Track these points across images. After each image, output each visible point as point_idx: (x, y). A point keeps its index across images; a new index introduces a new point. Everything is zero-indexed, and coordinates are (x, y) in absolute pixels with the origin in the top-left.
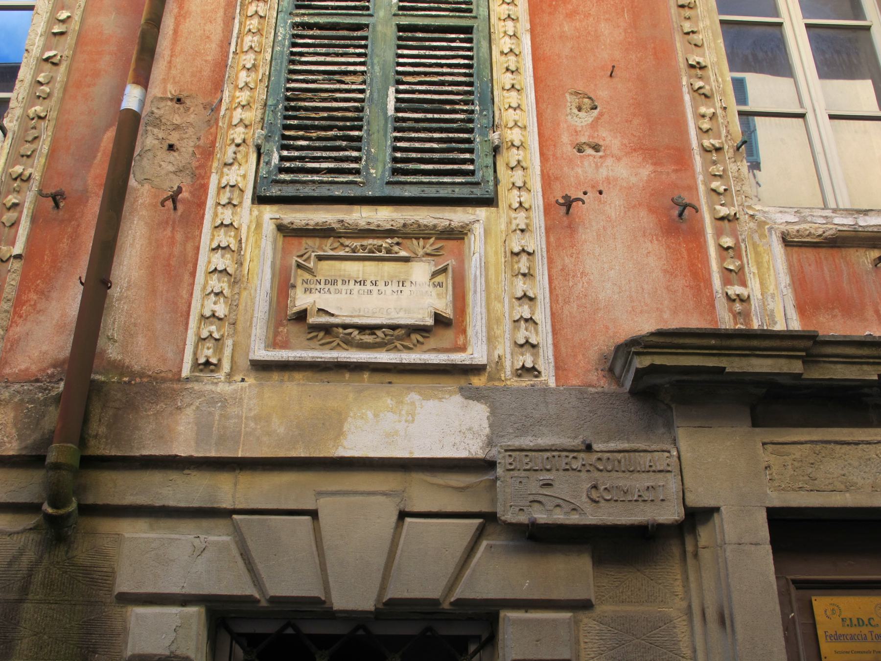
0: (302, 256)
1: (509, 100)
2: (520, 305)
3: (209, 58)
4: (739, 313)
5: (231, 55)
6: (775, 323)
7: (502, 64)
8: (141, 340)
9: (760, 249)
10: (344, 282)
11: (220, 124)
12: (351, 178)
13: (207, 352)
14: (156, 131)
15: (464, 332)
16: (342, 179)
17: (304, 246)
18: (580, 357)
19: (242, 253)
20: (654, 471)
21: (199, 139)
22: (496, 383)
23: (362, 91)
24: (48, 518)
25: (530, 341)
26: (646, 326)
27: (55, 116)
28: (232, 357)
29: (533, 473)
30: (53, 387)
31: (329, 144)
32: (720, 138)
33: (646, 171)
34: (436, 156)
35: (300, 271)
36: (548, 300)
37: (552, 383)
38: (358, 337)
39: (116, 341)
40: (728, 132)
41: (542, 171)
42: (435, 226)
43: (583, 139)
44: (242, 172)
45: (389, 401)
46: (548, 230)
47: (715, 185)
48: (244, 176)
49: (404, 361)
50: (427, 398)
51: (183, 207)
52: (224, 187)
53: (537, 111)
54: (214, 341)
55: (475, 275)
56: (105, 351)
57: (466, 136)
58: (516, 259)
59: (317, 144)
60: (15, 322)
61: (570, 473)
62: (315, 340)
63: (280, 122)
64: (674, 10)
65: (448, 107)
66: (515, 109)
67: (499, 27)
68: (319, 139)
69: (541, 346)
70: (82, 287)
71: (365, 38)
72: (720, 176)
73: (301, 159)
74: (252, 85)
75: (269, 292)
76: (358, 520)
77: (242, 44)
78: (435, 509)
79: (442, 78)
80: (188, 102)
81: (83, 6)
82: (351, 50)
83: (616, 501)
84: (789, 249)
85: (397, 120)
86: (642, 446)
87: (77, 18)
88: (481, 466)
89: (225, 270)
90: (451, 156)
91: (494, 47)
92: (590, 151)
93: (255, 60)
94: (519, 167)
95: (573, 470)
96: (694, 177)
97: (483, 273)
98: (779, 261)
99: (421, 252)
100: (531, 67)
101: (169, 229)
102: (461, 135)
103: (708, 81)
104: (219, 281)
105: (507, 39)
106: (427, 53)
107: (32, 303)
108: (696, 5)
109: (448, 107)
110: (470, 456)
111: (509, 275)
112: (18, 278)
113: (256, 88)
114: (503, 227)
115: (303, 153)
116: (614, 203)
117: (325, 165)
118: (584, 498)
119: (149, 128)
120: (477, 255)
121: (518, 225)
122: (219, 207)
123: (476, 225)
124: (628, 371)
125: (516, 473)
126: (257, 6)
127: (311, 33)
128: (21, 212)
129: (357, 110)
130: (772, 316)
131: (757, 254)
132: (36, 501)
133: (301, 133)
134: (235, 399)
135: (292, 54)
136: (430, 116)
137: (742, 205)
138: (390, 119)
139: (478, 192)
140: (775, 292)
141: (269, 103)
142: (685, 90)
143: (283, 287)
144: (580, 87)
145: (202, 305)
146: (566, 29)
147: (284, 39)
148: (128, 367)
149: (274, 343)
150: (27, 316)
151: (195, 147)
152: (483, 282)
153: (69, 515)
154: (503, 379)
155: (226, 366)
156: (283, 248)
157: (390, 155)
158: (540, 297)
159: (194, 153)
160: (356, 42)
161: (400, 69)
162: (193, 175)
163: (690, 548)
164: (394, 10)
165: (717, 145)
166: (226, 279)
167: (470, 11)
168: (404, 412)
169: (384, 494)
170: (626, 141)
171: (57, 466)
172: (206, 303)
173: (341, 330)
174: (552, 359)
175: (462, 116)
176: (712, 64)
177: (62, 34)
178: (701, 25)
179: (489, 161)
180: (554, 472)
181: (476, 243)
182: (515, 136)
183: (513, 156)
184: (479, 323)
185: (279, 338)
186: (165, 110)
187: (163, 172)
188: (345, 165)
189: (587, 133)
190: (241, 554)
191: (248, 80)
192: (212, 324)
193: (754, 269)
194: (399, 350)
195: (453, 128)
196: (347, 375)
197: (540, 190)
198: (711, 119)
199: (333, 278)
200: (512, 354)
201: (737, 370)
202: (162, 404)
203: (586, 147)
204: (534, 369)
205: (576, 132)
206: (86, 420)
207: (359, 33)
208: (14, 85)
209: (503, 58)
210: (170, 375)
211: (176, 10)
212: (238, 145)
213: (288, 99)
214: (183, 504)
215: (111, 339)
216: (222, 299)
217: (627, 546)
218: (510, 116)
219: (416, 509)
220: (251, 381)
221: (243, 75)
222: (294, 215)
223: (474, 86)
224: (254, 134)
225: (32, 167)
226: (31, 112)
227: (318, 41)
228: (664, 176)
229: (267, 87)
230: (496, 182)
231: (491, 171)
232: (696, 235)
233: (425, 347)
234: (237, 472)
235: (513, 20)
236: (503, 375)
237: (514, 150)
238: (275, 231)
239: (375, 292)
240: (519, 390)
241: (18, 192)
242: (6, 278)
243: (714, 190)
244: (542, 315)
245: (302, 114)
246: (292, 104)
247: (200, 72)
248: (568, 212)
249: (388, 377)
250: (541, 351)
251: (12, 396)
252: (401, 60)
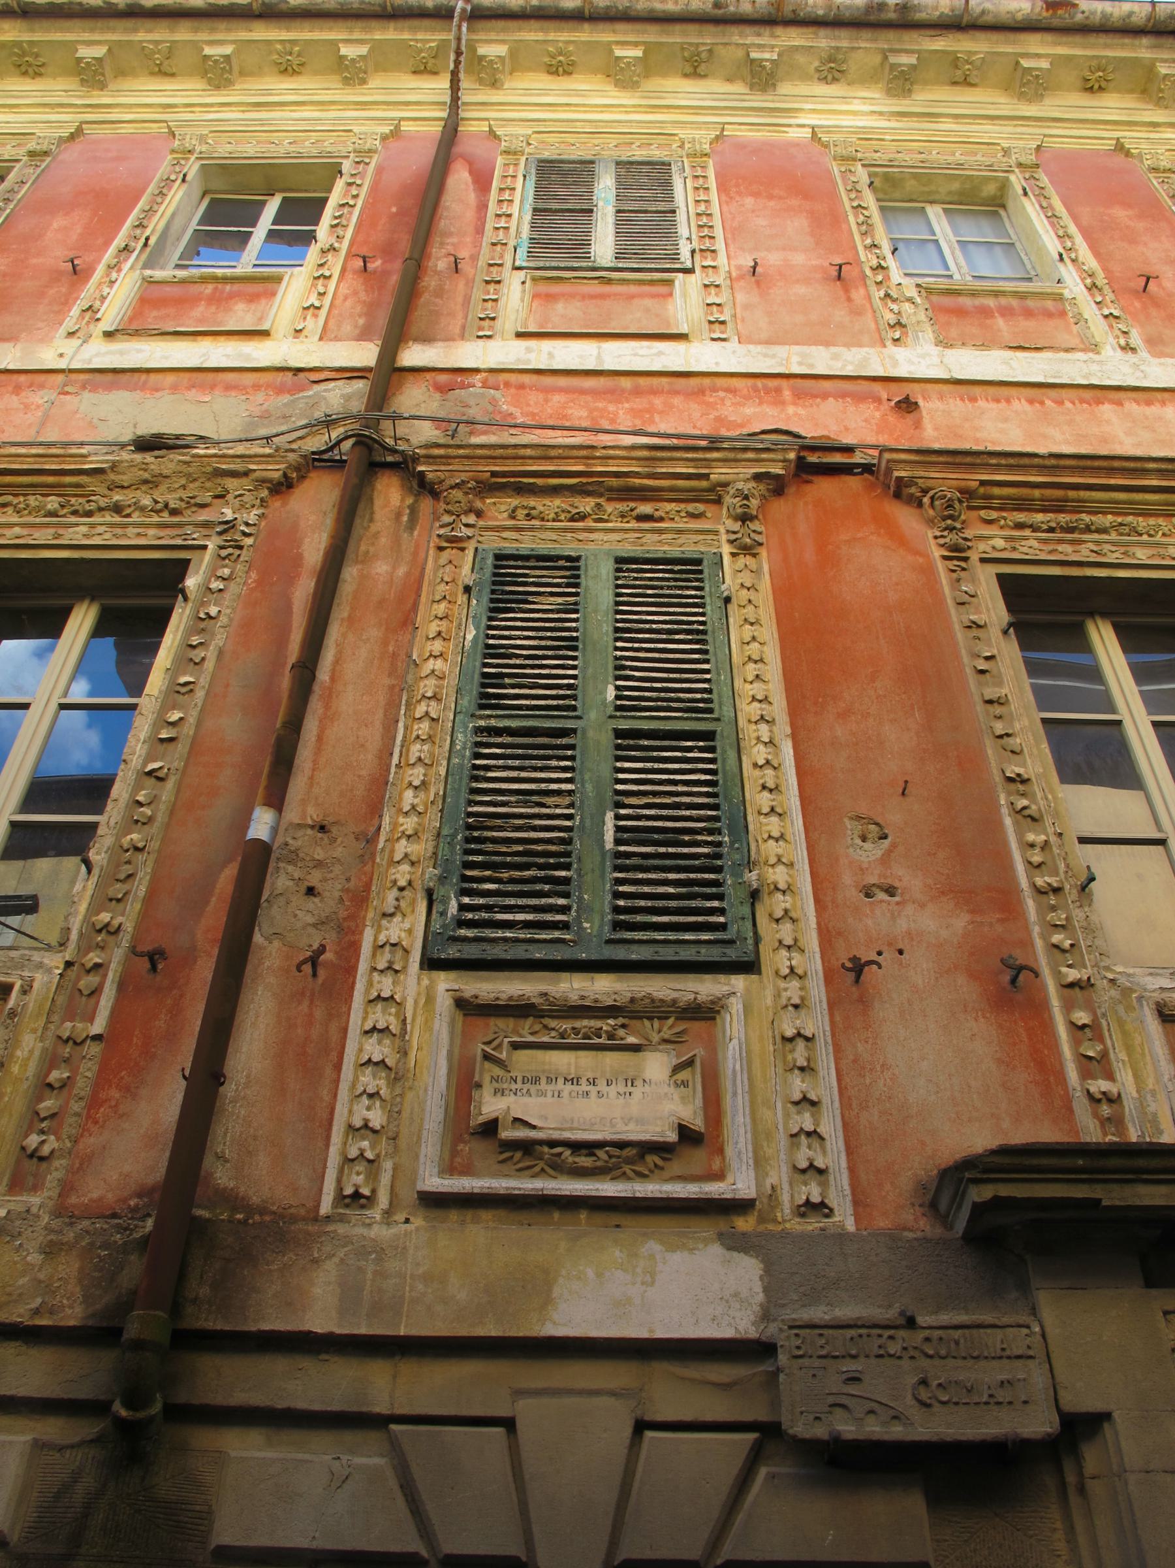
0: (489, 1043)
1: (768, 828)
2: (799, 1113)
3: (364, 773)
4: (1108, 1119)
5: (393, 769)
6: (1161, 1132)
7: (756, 781)
8: (263, 1161)
9: (1129, 1027)
10: (549, 1080)
11: (378, 860)
12: (557, 934)
13: (356, 1179)
14: (290, 868)
15: (721, 1151)
16: (544, 936)
17: (493, 1028)
18: (888, 1187)
19: (407, 1038)
20: (1009, 1357)
21: (348, 880)
22: (771, 1227)
23: (569, 817)
24: (120, 1422)
25: (816, 1163)
26: (980, 1140)
27: (156, 848)
28: (392, 1187)
29: (832, 1361)
30: (136, 1226)
31: (526, 888)
32: (1057, 875)
33: (961, 922)
34: (673, 904)
35: (487, 1065)
36: (837, 1104)
37: (850, 1226)
38: (570, 1160)
39: (227, 1161)
40: (1067, 866)
41: (819, 924)
42: (674, 1001)
43: (873, 880)
44: (407, 925)
45: (617, 1253)
46: (832, 1006)
47: (1056, 938)
48: (410, 931)
49: (638, 1195)
50: (672, 1248)
51: (326, 974)
52: (382, 946)
53: (807, 842)
54: (366, 1163)
55: (734, 1070)
56: (212, 1174)
57: (712, 876)
58: (789, 1046)
59: (510, 888)
60: (88, 1130)
61: (887, 1360)
62: (509, 1163)
63: (458, 859)
64: (980, 707)
65: (687, 838)
66: (778, 840)
67: (749, 732)
68: (512, 881)
69: (831, 1171)
70: (184, 1083)
71: (572, 747)
72: (1062, 926)
73: (488, 908)
74: (420, 809)
75: (445, 1093)
76: (576, 1433)
77: (407, 755)
78: (687, 1416)
79: (677, 799)
80: (334, 830)
81: (200, 705)
82: (554, 763)
83: (956, 1404)
84: (1168, 1025)
85: (618, 855)
86: (988, 1318)
87: (192, 720)
88: (753, 1350)
89: (383, 1061)
90: (693, 903)
91: (744, 758)
92: (882, 896)
93: (425, 775)
94: (787, 919)
95: (891, 1356)
96: (1027, 929)
97: (745, 1067)
98: (1157, 1043)
99: (655, 1038)
100: (795, 783)
101: (306, 1003)
102: (706, 876)
103: (1033, 800)
104: (374, 1076)
105: (761, 747)
106: (656, 766)
107: (113, 1103)
108: (1007, 700)
109: (687, 838)
110: (738, 1336)
111: (780, 1070)
112: (96, 1068)
113: (426, 812)
114: (769, 1001)
115: (491, 901)
116: (920, 967)
117: (520, 917)
118: (909, 1400)
119: (281, 865)
120: (735, 1042)
121: (789, 999)
122: (375, 974)
123: (733, 1000)
124: (960, 1206)
125: (806, 1362)
126: (428, 706)
127: (499, 740)
128: (105, 976)
129: (562, 841)
130: (1154, 1121)
131: (1125, 1034)
132: (102, 1397)
133: (488, 873)
134: (396, 1248)
135: (475, 767)
136: (662, 850)
137: (1096, 965)
138: (608, 854)
139: (732, 954)
140: (1156, 1087)
141: (445, 832)
142: (1005, 811)
143: (464, 1086)
144: (863, 808)
145: (350, 1111)
146: (839, 733)
147: (464, 748)
148: (243, 1198)
149: (450, 1168)
150: (105, 1122)
151: (342, 890)
152: (746, 1081)
153: (151, 1419)
154: (780, 1219)
155: (383, 1200)
156: (463, 1032)
157: (610, 902)
158: (826, 1101)
159: (341, 898)
160: (560, 752)
161: (619, 787)
162: (340, 929)
163: (1071, 1478)
164: (610, 710)
165: (1055, 885)
166: (383, 1075)
167: (711, 711)
168: (639, 1270)
169: (612, 1393)
170: (930, 881)
171: (138, 1345)
172: (355, 1107)
173: (546, 1149)
174: (848, 1192)
175: (705, 850)
176: (1037, 776)
177: (171, 740)
178: (1017, 726)
179: (746, 910)
180: (862, 1359)
181: (733, 1024)
182: (779, 875)
183: (779, 903)
184: (742, 1140)
185: (458, 1160)
186: (303, 840)
187: (299, 925)
188: (549, 917)
189: (877, 872)
190: (401, 1487)
191: (416, 801)
192: (363, 1139)
193: (1123, 1056)
194: (629, 1179)
195: (694, 866)
196: (556, 1215)
197: (817, 949)
198: (1042, 849)
199: (534, 1075)
200: (791, 1184)
201: (1118, 1203)
202: (291, 1255)
203: (877, 891)
204: (823, 1204)
205: (862, 870)
206: (182, 1276)
207: (564, 741)
208: (105, 805)
209: (757, 772)
210: (302, 1212)
211: (321, 711)
212: (402, 889)
213: (469, 827)
214: (317, 1407)
215: (220, 1157)
216: (378, 1103)
217: (977, 1476)
218: (772, 849)
219: (659, 1418)
220: (418, 1222)
221: (409, 794)
222: (479, 986)
223: (722, 810)
224: (423, 873)
225: (123, 915)
226: (126, 841)
227: (509, 751)
228: (986, 929)
229: (441, 811)
230: (757, 939)
231: (749, 924)
232: (1038, 1008)
233: (666, 1174)
234: (397, 1358)
235: (768, 722)
236: (779, 1215)
237: (779, 896)
238: (453, 1008)
239: (593, 1094)
240: (803, 1236)
241: (103, 948)
242: (79, 1067)
243: (1056, 946)
244: (830, 1125)
245: (489, 847)
246: (476, 834)
247: (351, 790)
248: (857, 980)
249: (615, 1218)
250: (831, 1178)
251: (78, 1238)
252: (621, 776)
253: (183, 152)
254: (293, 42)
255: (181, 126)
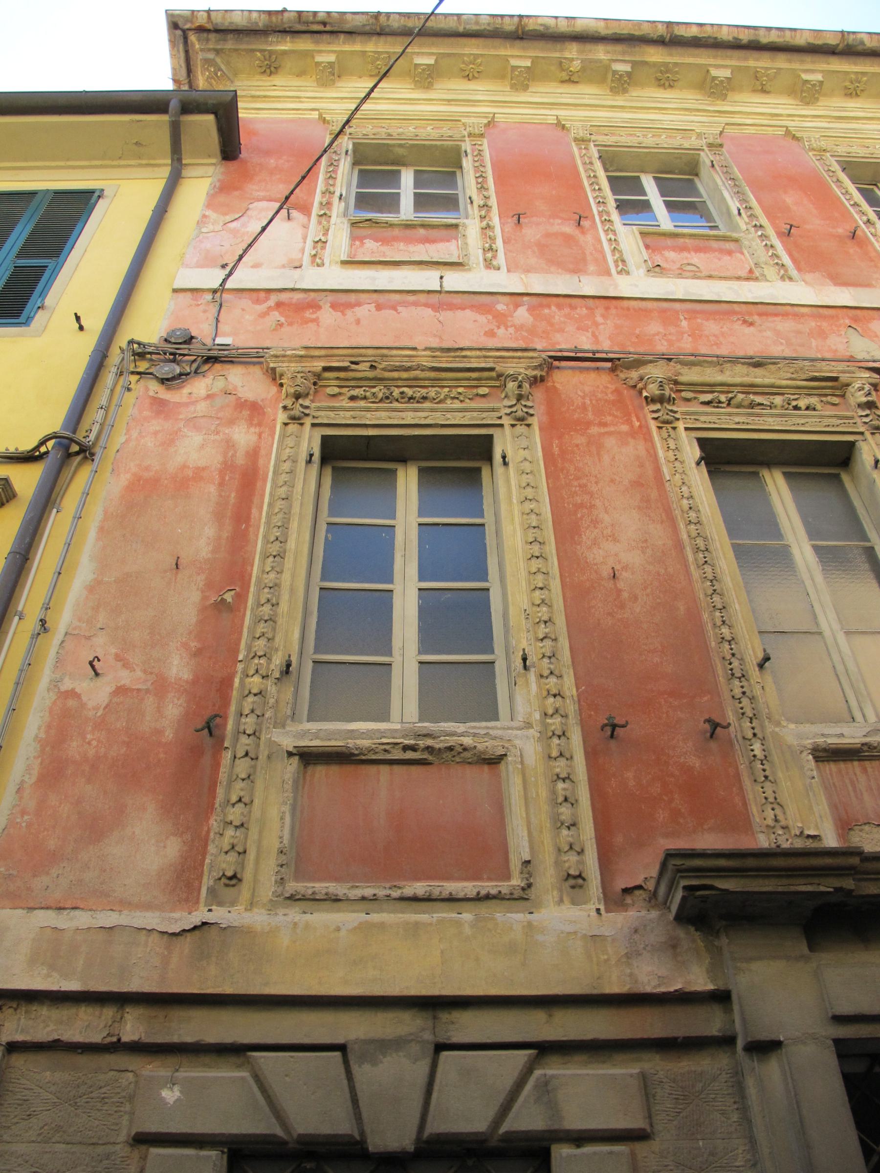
253: (820, 151)
254: (864, 74)
255: (799, 131)
